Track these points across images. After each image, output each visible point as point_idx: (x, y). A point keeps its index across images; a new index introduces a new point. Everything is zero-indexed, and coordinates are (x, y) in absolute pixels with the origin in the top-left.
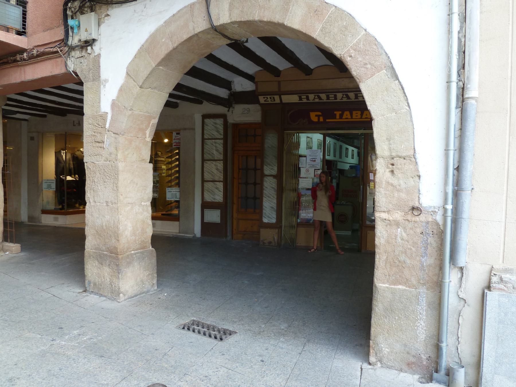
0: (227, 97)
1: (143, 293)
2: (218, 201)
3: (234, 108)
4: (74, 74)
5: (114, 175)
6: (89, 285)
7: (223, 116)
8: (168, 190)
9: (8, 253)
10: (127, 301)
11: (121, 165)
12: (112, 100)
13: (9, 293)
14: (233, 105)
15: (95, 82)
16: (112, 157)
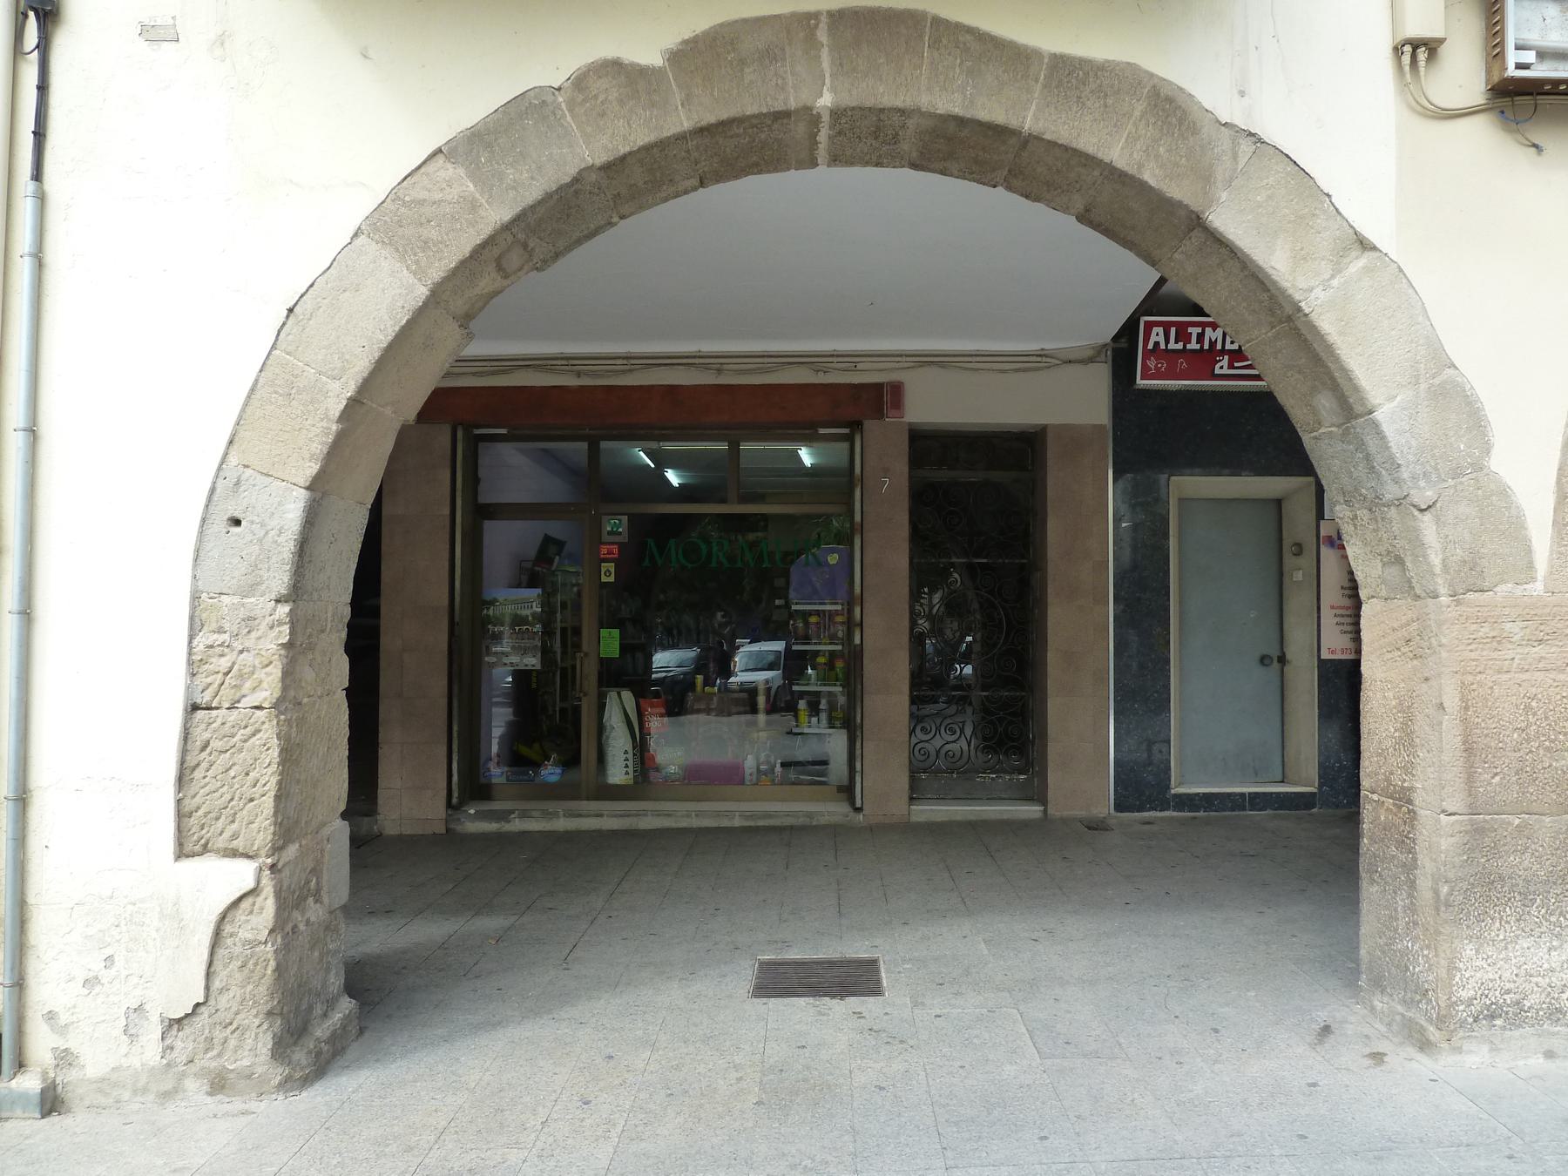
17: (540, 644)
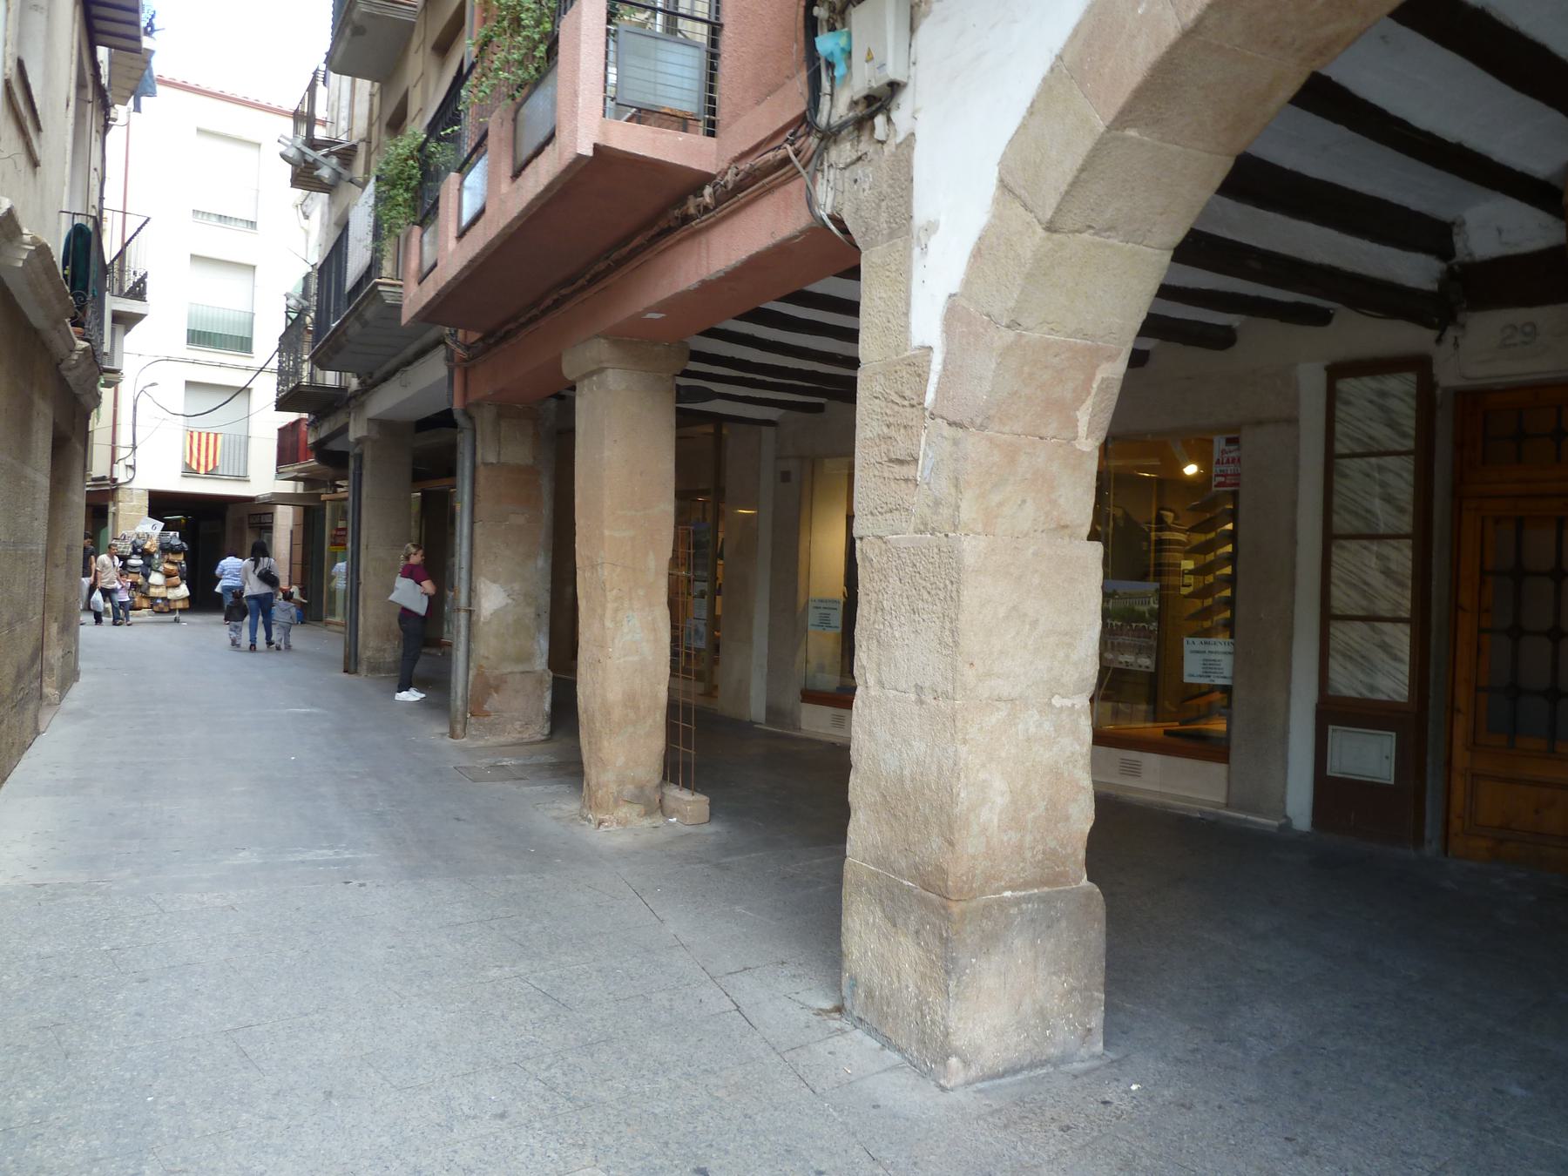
0: (1434, 287)
1: (1043, 1064)
2: (1389, 696)
3: (1463, 326)
4: (833, 227)
5: (946, 586)
6: (853, 993)
7: (1419, 364)
8: (1191, 646)
9: (675, 819)
10: (973, 1088)
11: (971, 548)
12: (947, 295)
13: (614, 969)
14: (1461, 317)
15: (895, 240)
16: (940, 518)
17: (1155, 644)
